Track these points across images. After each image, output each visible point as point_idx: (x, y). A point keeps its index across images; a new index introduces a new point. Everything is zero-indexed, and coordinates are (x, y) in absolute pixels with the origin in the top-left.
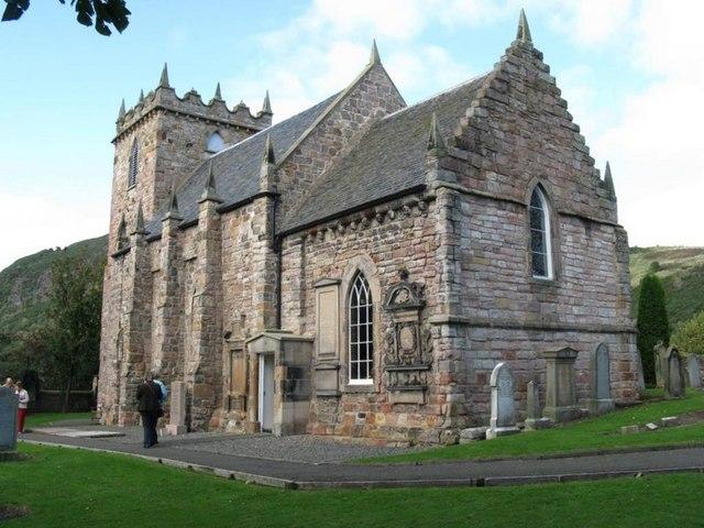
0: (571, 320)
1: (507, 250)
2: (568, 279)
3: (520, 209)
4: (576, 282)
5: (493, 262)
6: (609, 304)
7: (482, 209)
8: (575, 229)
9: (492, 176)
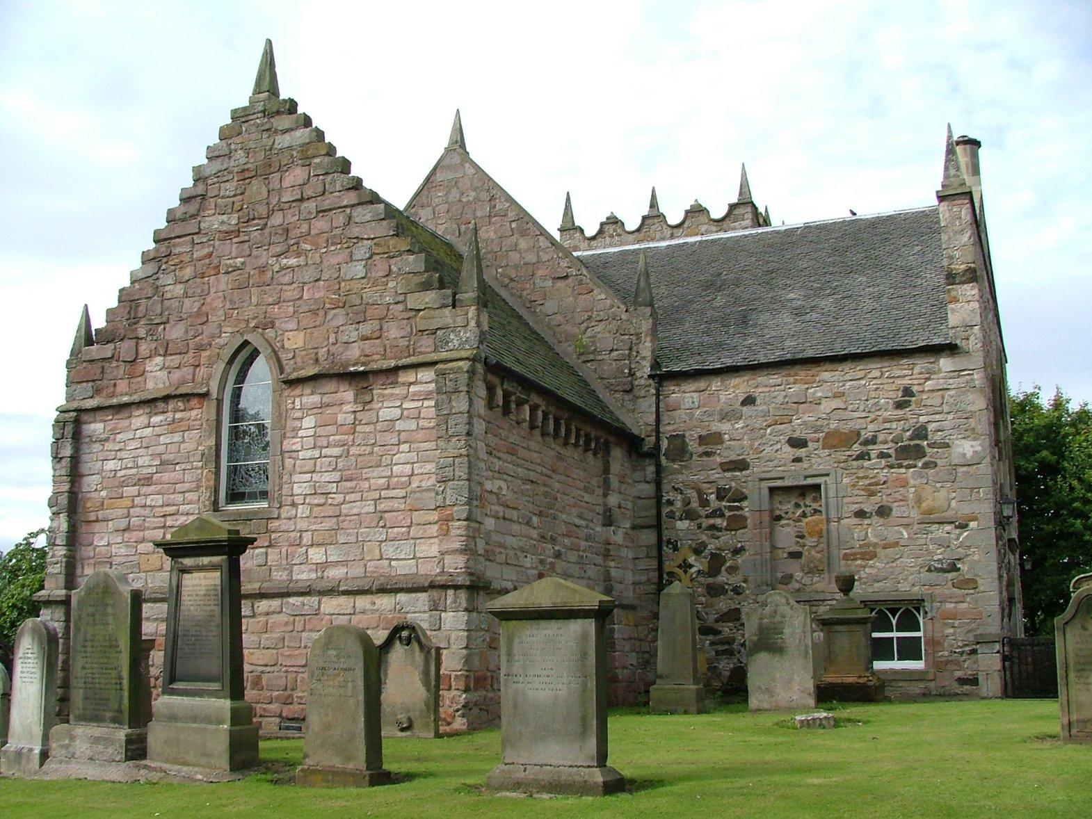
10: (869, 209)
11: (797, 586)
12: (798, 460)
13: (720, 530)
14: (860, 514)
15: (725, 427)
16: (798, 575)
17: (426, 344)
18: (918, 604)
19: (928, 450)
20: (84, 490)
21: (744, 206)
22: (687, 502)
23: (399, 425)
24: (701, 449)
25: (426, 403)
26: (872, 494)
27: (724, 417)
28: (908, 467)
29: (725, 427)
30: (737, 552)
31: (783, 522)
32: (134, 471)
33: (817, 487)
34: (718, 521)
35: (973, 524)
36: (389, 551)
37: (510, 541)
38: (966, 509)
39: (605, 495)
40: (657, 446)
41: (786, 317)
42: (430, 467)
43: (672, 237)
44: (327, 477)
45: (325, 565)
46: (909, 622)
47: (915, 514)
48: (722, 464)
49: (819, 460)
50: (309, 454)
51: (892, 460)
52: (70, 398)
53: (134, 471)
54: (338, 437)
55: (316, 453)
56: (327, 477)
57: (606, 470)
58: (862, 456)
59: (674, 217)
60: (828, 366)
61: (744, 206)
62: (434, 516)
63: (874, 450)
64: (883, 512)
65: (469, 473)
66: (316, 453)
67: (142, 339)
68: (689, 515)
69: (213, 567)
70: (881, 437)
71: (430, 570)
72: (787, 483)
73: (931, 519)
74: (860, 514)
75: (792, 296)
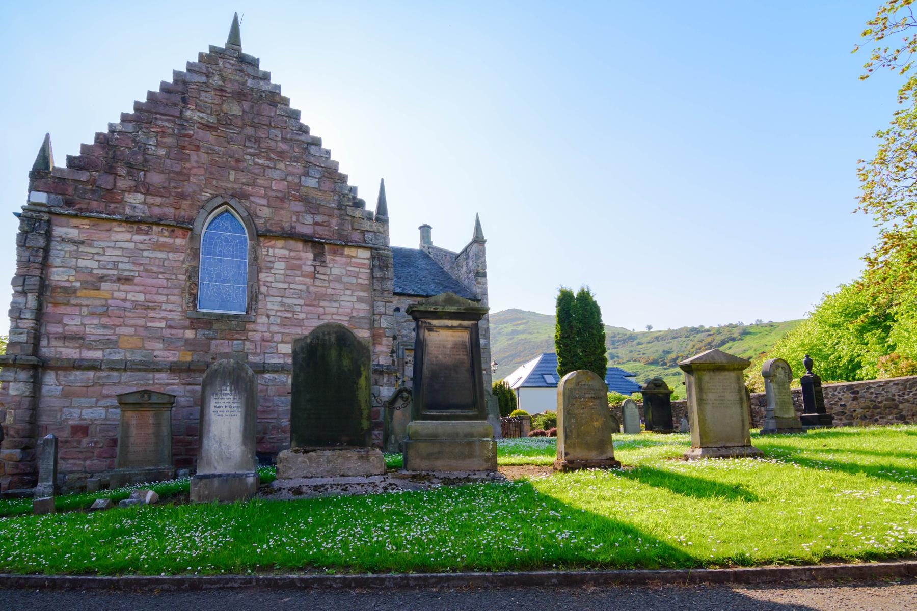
10: (537, 312)
20: (52, 278)
25: (362, 270)
32: (115, 272)
44: (295, 301)
50: (280, 285)
53: (115, 272)
54: (301, 279)
55: (286, 286)
56: (295, 301)
65: (20, 514)
66: (286, 286)
67: (120, 176)
69: (465, 328)
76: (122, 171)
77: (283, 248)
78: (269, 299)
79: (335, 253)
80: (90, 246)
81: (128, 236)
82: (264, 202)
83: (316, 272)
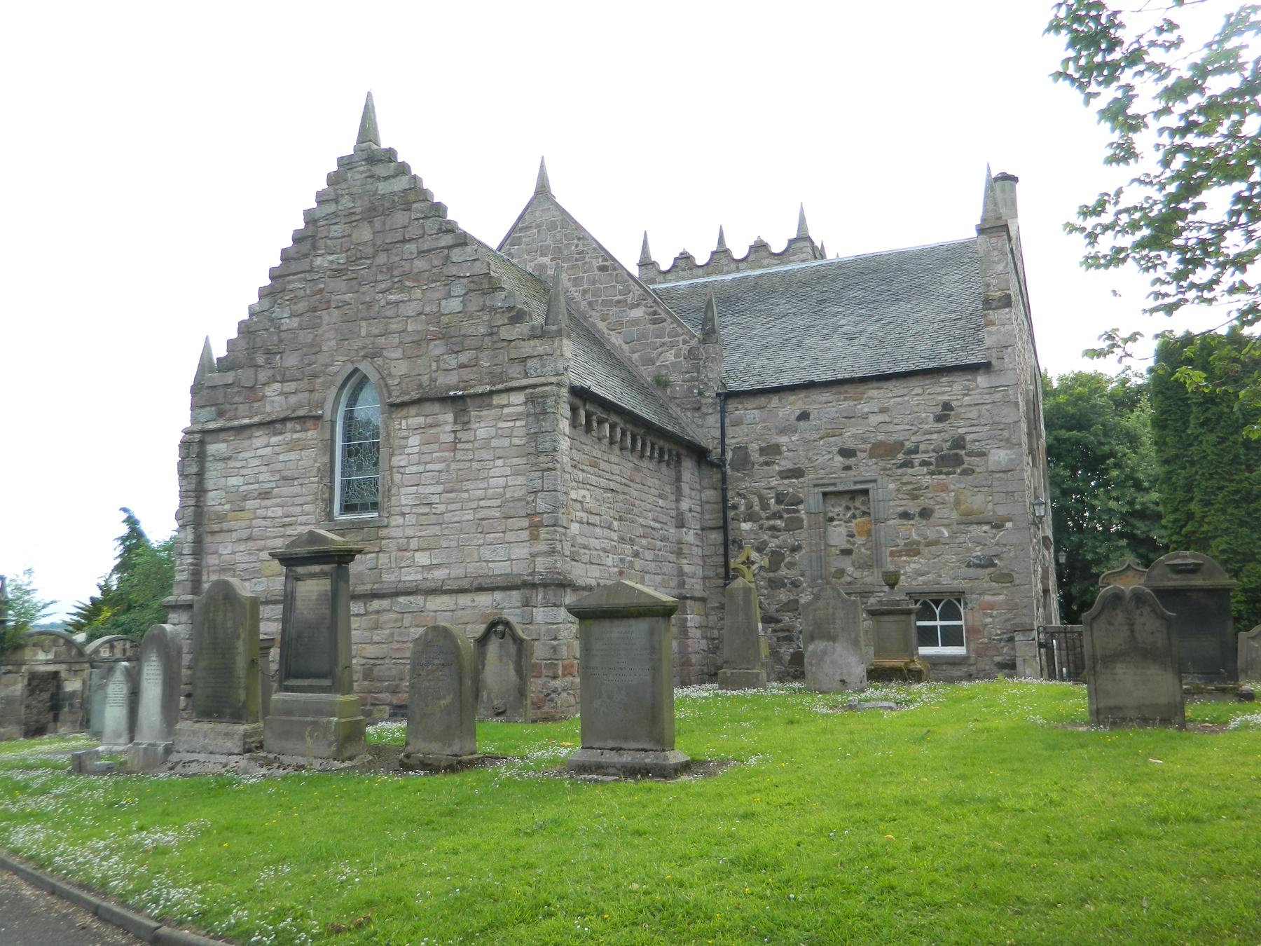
0: (411, 577)
1: (286, 491)
2: (406, 510)
3: (310, 424)
4: (426, 510)
5: (261, 512)
6: (510, 536)
7: (246, 443)
8: (430, 420)
9: (272, 390)
11: (849, 579)
12: (848, 468)
13: (779, 530)
14: (905, 515)
15: (783, 439)
16: (850, 569)
17: (515, 370)
18: (959, 596)
19: (966, 459)
21: (802, 239)
22: (750, 506)
23: (495, 443)
24: (762, 459)
25: (518, 423)
26: (915, 498)
27: (782, 431)
28: (948, 474)
29: (783, 439)
30: (795, 549)
31: (836, 523)
32: (256, 486)
33: (866, 492)
34: (778, 523)
35: (1009, 525)
36: (487, 553)
37: (593, 543)
38: (1002, 511)
39: (678, 501)
40: (723, 461)
41: (837, 342)
42: (520, 480)
43: (738, 270)
45: (429, 568)
46: (951, 612)
47: (955, 515)
48: (780, 473)
49: (867, 468)
51: (933, 468)
52: (194, 420)
53: (256, 486)
55: (421, 468)
57: (678, 479)
58: (908, 464)
59: (739, 252)
60: (875, 384)
61: (802, 239)
62: (525, 523)
63: (917, 458)
64: (925, 513)
66: (421, 468)
68: (751, 517)
70: (922, 447)
71: (520, 569)
72: (840, 488)
73: (970, 519)
74: (905, 515)
75: (843, 322)
76: (260, 360)
77: (417, 415)
78: (404, 490)
79: (481, 408)
80: (236, 459)
81: (264, 440)
82: (398, 354)
83: (456, 441)
